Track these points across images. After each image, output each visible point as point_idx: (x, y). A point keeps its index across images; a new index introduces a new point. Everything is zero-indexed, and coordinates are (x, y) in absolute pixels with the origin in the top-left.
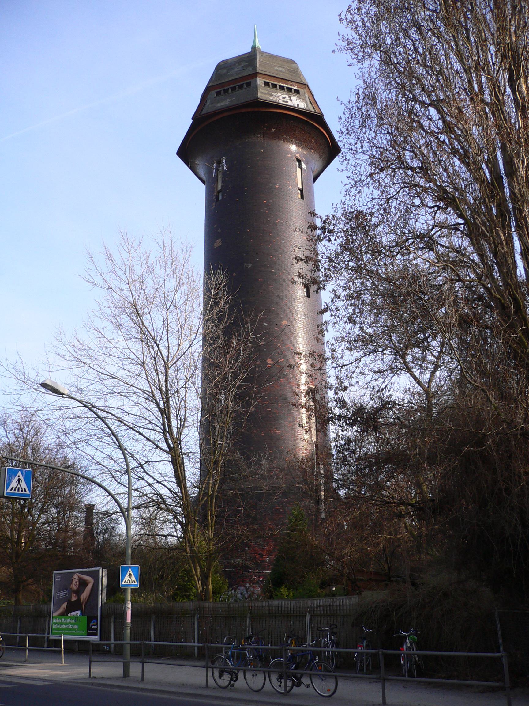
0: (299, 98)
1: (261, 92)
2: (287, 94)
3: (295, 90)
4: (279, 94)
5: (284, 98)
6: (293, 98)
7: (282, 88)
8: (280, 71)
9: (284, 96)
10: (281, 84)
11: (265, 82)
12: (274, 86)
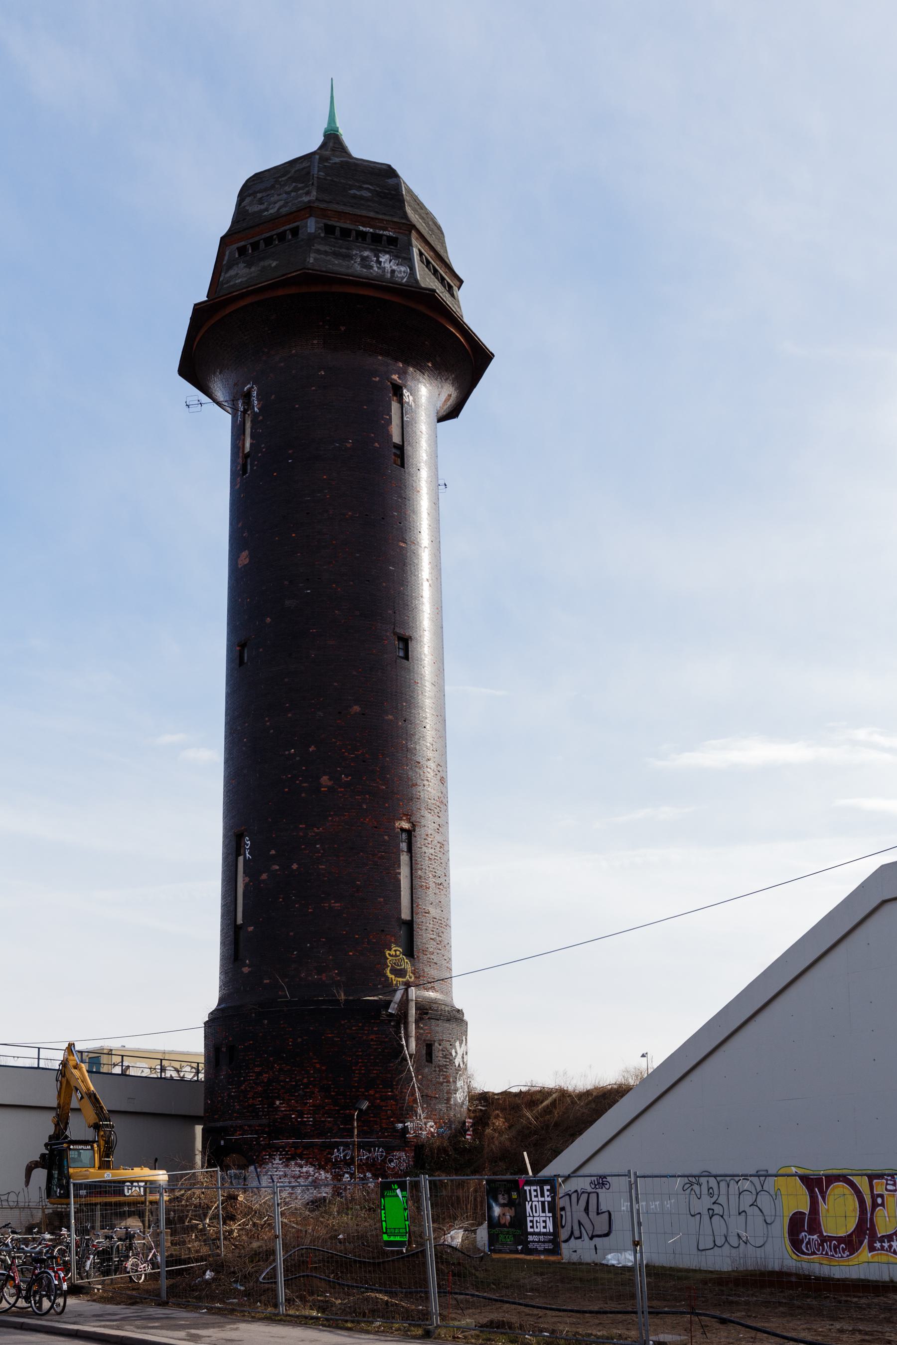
0: (397, 257)
1: (318, 252)
2: (372, 250)
3: (389, 237)
4: (354, 252)
5: (364, 259)
6: (384, 258)
7: (363, 235)
8: (361, 198)
9: (366, 253)
10: (361, 228)
11: (326, 225)
12: (346, 233)
